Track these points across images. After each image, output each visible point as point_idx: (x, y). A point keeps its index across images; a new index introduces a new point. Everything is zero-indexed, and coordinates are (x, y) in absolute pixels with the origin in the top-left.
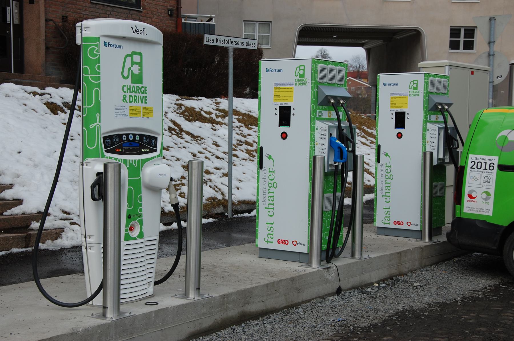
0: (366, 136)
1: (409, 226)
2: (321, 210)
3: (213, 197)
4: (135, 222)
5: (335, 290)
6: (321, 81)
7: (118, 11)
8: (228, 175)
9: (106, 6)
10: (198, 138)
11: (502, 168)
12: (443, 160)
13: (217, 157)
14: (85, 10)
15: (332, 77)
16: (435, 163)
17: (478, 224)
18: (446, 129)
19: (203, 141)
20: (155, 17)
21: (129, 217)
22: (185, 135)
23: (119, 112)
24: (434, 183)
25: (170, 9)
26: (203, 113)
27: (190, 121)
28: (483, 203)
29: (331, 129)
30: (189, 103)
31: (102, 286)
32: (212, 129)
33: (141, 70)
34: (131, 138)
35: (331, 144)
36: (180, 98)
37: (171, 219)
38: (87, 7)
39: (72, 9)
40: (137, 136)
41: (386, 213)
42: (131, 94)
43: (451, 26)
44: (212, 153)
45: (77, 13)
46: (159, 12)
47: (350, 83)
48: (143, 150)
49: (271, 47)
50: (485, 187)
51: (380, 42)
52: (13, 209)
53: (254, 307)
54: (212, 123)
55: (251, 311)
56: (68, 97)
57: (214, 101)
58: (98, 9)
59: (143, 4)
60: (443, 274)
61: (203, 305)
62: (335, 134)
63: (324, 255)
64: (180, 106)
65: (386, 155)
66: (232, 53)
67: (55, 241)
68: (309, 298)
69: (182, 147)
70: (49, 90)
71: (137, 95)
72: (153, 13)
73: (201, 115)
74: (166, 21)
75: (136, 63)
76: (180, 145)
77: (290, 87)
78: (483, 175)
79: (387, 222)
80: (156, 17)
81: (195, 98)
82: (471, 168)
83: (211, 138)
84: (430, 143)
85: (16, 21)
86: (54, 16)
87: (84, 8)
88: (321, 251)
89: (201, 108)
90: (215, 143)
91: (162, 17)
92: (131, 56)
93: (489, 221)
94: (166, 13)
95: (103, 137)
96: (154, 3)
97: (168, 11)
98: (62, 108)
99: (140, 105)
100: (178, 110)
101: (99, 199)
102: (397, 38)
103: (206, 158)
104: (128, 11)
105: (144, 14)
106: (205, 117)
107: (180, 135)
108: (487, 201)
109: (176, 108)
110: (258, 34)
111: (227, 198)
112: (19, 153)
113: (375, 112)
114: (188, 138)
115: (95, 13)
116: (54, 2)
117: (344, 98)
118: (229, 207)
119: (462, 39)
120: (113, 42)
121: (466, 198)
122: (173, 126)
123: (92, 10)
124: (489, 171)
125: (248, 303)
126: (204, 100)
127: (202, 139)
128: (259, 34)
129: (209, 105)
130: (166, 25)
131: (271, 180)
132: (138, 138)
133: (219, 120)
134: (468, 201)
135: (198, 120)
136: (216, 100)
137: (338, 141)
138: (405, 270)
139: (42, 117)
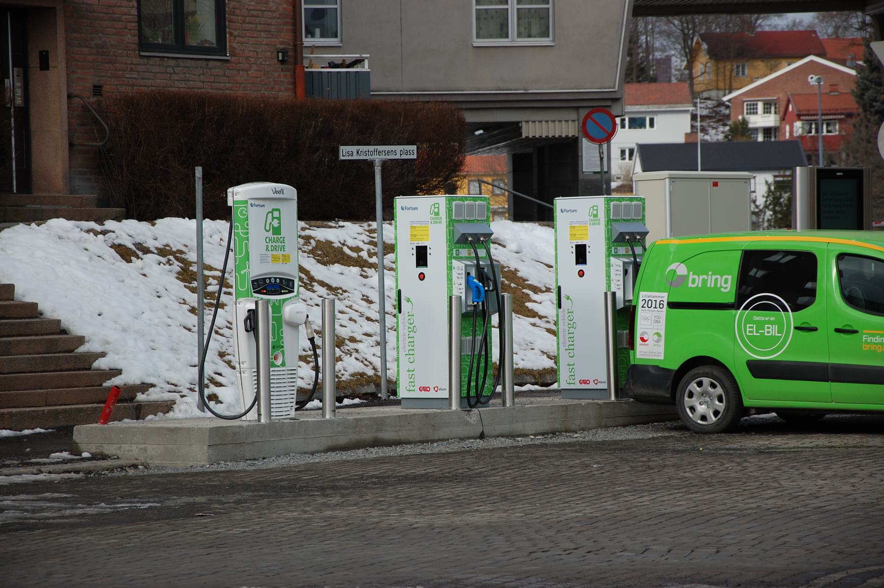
1: (596, 384)
2: (459, 354)
3: (361, 372)
5: (478, 434)
6: (457, 218)
7: (187, 65)
8: (382, 344)
9: (166, 59)
10: (338, 291)
11: (672, 305)
13: (368, 319)
14: (131, 70)
17: (651, 369)
19: (346, 294)
20: (254, 67)
21: (274, 347)
22: (317, 287)
23: (263, 259)
25: (281, 50)
26: (346, 249)
27: (325, 264)
28: (655, 345)
29: (468, 268)
30: (322, 234)
31: (257, 399)
32: (361, 275)
33: (279, 223)
34: (273, 281)
36: (308, 226)
37: (302, 397)
38: (134, 64)
39: (109, 72)
40: (278, 279)
41: (570, 370)
42: (272, 244)
44: (360, 313)
45: (118, 77)
46: (261, 58)
48: (283, 291)
49: (554, 41)
50: (656, 327)
52: (113, 379)
54: (362, 266)
55: (384, 438)
56: (139, 235)
57: (366, 228)
58: (153, 65)
59: (231, 47)
60: (110, 156)
62: (473, 273)
64: (307, 239)
65: (568, 298)
66: (380, 168)
67: (167, 415)
68: (446, 438)
69: (313, 304)
70: (110, 224)
71: (277, 244)
72: (250, 61)
73: (343, 253)
74: (274, 73)
75: (276, 218)
76: (310, 302)
77: (426, 225)
78: (653, 315)
79: (572, 381)
80: (254, 67)
82: (642, 307)
83: (359, 291)
86: (80, 88)
88: (461, 398)
89: (342, 242)
90: (365, 297)
91: (266, 67)
92: (272, 212)
93: (661, 366)
94: (274, 59)
95: (252, 281)
96: (251, 42)
97: (278, 52)
98: (135, 252)
99: (280, 253)
100: (305, 247)
101: (251, 331)
103: (351, 319)
104: (203, 63)
105: (234, 65)
106: (349, 257)
107: (310, 287)
108: (659, 344)
109: (301, 244)
110: (516, 7)
111: (380, 374)
112: (99, 315)
114: (322, 291)
115: (147, 74)
116: (80, 63)
118: (382, 386)
120: (257, 202)
121: (638, 341)
123: (141, 68)
124: (659, 309)
126: (348, 226)
127: (345, 291)
130: (274, 81)
131: (410, 324)
132: (278, 281)
133: (374, 260)
134: (641, 345)
135: (338, 262)
136: (369, 225)
137: (475, 280)
138: (573, 427)
139: (113, 267)
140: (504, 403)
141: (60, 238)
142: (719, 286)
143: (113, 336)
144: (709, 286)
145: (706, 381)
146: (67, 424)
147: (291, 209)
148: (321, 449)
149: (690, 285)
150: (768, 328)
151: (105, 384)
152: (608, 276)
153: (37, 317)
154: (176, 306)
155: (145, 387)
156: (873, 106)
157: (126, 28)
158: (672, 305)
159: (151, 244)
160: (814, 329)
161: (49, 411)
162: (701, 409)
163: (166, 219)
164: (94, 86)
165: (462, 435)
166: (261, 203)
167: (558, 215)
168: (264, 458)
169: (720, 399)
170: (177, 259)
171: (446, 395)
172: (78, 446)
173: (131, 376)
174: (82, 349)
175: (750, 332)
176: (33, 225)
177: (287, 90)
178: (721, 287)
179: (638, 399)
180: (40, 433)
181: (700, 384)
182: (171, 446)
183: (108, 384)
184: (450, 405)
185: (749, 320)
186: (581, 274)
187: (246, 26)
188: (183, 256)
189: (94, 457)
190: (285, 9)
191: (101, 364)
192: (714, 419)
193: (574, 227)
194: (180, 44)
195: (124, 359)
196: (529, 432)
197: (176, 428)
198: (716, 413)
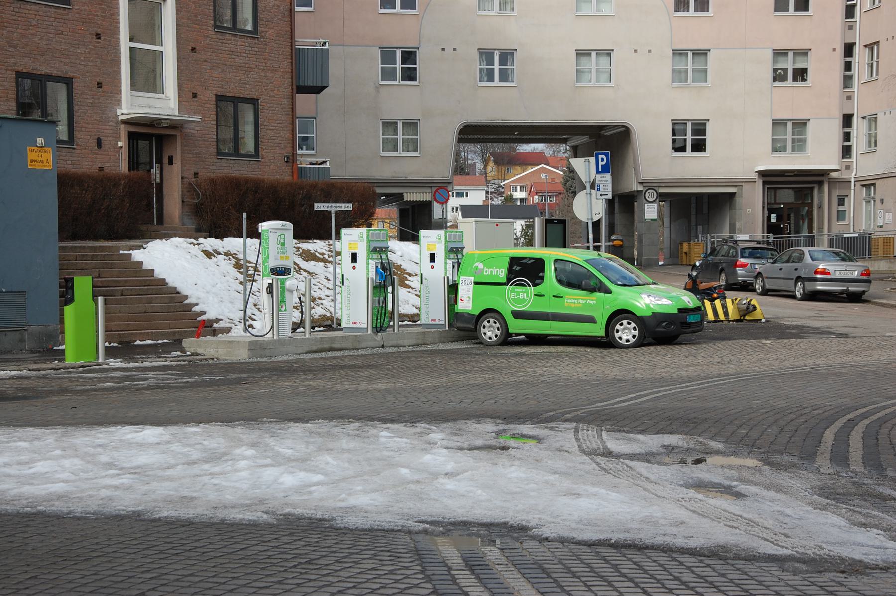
4: (283, 304)
5: (381, 345)
8: (334, 301)
11: (476, 283)
13: (328, 288)
17: (466, 315)
19: (317, 276)
20: (273, 164)
22: (302, 272)
26: (317, 254)
31: (272, 327)
49: (420, 154)
53: (336, 345)
54: (324, 263)
61: (312, 340)
62: (379, 267)
64: (298, 248)
70: (201, 240)
76: (299, 280)
81: (310, 241)
85: (158, 180)
106: (318, 257)
113: (586, 241)
114: (305, 274)
119: (689, 138)
120: (273, 230)
121: (459, 300)
123: (217, 164)
125: (333, 343)
133: (331, 259)
138: (427, 342)
140: (394, 330)
141: (177, 247)
143: (202, 295)
147: (291, 233)
149: (485, 274)
155: (217, 320)
158: (476, 283)
160: (543, 296)
162: (489, 334)
166: (276, 231)
169: (498, 329)
170: (234, 258)
173: (210, 315)
174: (187, 302)
176: (164, 240)
181: (489, 322)
183: (199, 319)
184: (368, 331)
185: (513, 291)
189: (192, 355)
192: (495, 339)
194: (236, 152)
198: (496, 336)
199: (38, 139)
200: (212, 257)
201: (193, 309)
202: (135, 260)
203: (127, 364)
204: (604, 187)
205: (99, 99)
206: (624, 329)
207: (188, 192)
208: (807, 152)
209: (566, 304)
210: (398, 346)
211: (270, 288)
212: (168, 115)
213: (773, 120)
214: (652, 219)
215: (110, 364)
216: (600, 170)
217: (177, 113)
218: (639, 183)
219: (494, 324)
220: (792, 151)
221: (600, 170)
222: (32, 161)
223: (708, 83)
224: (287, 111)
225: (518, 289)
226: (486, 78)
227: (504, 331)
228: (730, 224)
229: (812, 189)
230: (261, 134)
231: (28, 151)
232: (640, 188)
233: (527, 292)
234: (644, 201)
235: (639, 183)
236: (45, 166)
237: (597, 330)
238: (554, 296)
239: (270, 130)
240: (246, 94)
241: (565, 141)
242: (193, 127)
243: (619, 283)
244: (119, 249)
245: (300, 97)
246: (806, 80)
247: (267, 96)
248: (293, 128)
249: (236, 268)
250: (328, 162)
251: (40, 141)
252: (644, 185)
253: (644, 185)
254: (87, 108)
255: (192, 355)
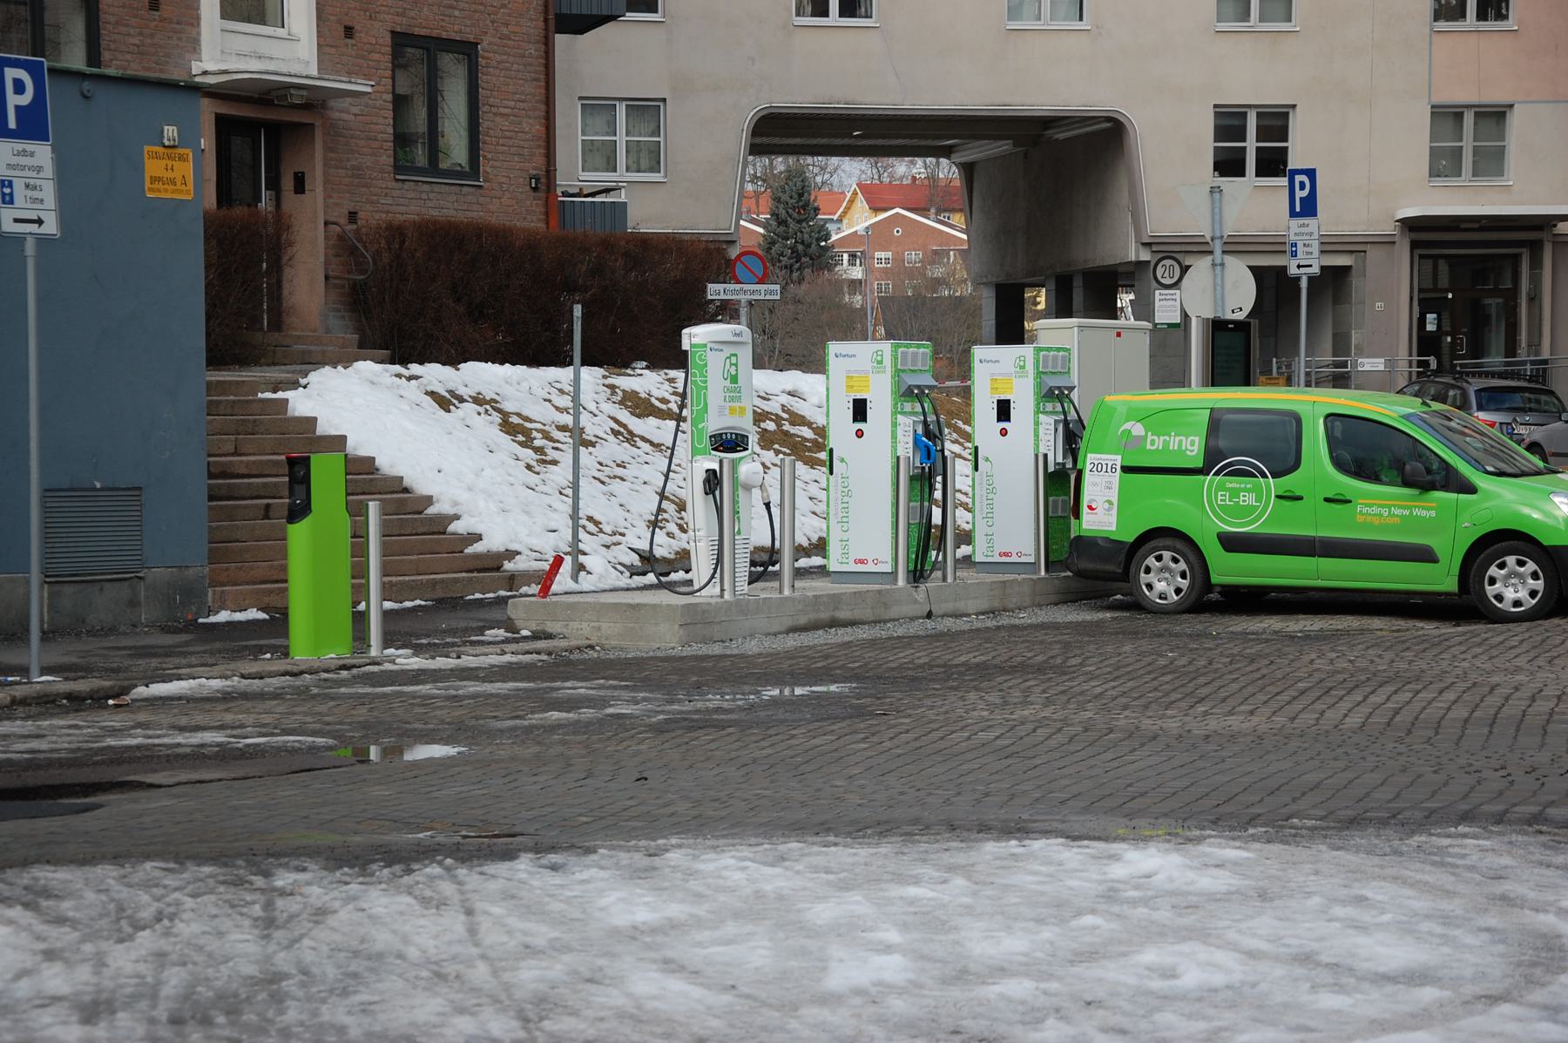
0: (961, 440)
5: (925, 614)
11: (1126, 469)
12: (1064, 464)
15: (914, 363)
16: (1051, 469)
17: (1100, 542)
18: (1066, 423)
20: (508, 195)
22: (640, 443)
23: (721, 413)
24: (1051, 499)
26: (653, 400)
27: (639, 416)
35: (916, 441)
43: (1216, 106)
47: (897, 232)
51: (1003, 147)
53: (843, 614)
57: (664, 376)
59: (485, 171)
61: (799, 602)
62: (920, 431)
63: (911, 575)
64: (612, 387)
70: (415, 368)
76: (640, 460)
79: (989, 554)
84: (1044, 442)
87: (384, 191)
88: (908, 572)
92: (729, 358)
97: (531, 179)
99: (736, 405)
102: (1058, 136)
104: (457, 189)
106: (660, 410)
110: (625, 138)
117: (929, 387)
119: (1251, 145)
120: (716, 346)
121: (1084, 510)
122: (616, 427)
123: (396, 193)
128: (628, 139)
129: (659, 385)
130: (527, 210)
132: (734, 436)
137: (924, 439)
138: (1011, 606)
140: (944, 579)
141: (373, 383)
142: (1184, 448)
143: (463, 496)
144: (1171, 448)
145: (1167, 555)
146: (444, 595)
147: (746, 355)
148: (783, 629)
149: (1148, 447)
150: (1244, 496)
151: (466, 551)
152: (1036, 435)
153: (373, 473)
154: (513, 462)
155: (511, 554)
156: (780, 261)
157: (382, 148)
158: (1126, 469)
159: (462, 391)
160: (1300, 498)
161: (428, 580)
162: (1160, 586)
163: (469, 363)
164: (350, 213)
165: (910, 615)
166: (720, 347)
167: (833, 363)
168: (731, 640)
169: (1183, 576)
170: (495, 409)
171: (888, 568)
172: (513, 623)
173: (493, 542)
174: (431, 510)
175: (1221, 500)
176: (340, 368)
177: (539, 220)
178: (1187, 449)
179: (1080, 574)
180: (420, 606)
181: (1159, 558)
182: (632, 625)
183: (469, 550)
184: (896, 580)
185: (1220, 487)
186: (1004, 432)
187: (500, 148)
188: (498, 405)
189: (536, 636)
190: (538, 130)
191: (455, 527)
192: (1176, 598)
193: (852, 377)
194: (433, 168)
195: (482, 522)
196: (972, 612)
197: (638, 605)
198: (1178, 591)
199: (166, 128)
200: (451, 407)
201: (453, 528)
202: (297, 414)
203: (430, 661)
204: (1306, 249)
205: (152, 36)
206: (1509, 576)
207: (337, 256)
208: (1505, 177)
209: (1360, 519)
210: (957, 615)
211: (712, 482)
212: (307, 77)
213: (1433, 107)
214: (1170, 325)
215: (398, 661)
216: (1298, 209)
217: (315, 73)
218: (1144, 244)
219: (1173, 565)
220: (1474, 176)
221: (1298, 209)
222: (154, 179)
223: (1293, 23)
224: (536, 72)
225: (1234, 483)
226: (809, 9)
227: (1199, 580)
228: (1335, 336)
229: (1516, 259)
230: (484, 124)
231: (146, 156)
232: (1145, 256)
233: (1257, 490)
234: (1154, 284)
235: (1144, 244)
236: (180, 191)
237: (1442, 578)
238: (1327, 500)
239: (502, 115)
240: (452, 31)
241: (947, 152)
242: (346, 105)
243: (1490, 469)
244: (255, 387)
245: (561, 40)
246: (1505, 17)
247: (493, 36)
248: (547, 112)
249: (507, 433)
250: (623, 190)
251: (170, 131)
252: (1155, 248)
253: (1155, 248)
254: (129, 57)
255: (536, 636)
